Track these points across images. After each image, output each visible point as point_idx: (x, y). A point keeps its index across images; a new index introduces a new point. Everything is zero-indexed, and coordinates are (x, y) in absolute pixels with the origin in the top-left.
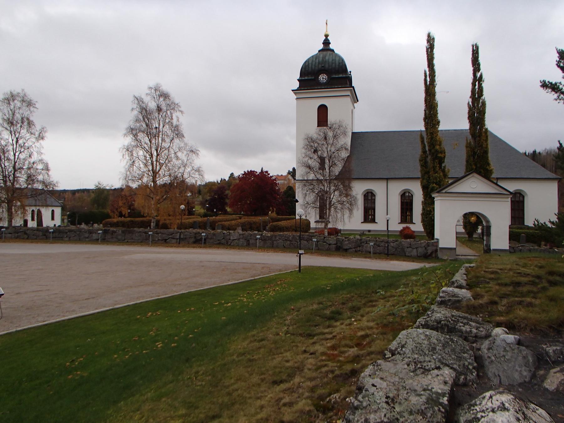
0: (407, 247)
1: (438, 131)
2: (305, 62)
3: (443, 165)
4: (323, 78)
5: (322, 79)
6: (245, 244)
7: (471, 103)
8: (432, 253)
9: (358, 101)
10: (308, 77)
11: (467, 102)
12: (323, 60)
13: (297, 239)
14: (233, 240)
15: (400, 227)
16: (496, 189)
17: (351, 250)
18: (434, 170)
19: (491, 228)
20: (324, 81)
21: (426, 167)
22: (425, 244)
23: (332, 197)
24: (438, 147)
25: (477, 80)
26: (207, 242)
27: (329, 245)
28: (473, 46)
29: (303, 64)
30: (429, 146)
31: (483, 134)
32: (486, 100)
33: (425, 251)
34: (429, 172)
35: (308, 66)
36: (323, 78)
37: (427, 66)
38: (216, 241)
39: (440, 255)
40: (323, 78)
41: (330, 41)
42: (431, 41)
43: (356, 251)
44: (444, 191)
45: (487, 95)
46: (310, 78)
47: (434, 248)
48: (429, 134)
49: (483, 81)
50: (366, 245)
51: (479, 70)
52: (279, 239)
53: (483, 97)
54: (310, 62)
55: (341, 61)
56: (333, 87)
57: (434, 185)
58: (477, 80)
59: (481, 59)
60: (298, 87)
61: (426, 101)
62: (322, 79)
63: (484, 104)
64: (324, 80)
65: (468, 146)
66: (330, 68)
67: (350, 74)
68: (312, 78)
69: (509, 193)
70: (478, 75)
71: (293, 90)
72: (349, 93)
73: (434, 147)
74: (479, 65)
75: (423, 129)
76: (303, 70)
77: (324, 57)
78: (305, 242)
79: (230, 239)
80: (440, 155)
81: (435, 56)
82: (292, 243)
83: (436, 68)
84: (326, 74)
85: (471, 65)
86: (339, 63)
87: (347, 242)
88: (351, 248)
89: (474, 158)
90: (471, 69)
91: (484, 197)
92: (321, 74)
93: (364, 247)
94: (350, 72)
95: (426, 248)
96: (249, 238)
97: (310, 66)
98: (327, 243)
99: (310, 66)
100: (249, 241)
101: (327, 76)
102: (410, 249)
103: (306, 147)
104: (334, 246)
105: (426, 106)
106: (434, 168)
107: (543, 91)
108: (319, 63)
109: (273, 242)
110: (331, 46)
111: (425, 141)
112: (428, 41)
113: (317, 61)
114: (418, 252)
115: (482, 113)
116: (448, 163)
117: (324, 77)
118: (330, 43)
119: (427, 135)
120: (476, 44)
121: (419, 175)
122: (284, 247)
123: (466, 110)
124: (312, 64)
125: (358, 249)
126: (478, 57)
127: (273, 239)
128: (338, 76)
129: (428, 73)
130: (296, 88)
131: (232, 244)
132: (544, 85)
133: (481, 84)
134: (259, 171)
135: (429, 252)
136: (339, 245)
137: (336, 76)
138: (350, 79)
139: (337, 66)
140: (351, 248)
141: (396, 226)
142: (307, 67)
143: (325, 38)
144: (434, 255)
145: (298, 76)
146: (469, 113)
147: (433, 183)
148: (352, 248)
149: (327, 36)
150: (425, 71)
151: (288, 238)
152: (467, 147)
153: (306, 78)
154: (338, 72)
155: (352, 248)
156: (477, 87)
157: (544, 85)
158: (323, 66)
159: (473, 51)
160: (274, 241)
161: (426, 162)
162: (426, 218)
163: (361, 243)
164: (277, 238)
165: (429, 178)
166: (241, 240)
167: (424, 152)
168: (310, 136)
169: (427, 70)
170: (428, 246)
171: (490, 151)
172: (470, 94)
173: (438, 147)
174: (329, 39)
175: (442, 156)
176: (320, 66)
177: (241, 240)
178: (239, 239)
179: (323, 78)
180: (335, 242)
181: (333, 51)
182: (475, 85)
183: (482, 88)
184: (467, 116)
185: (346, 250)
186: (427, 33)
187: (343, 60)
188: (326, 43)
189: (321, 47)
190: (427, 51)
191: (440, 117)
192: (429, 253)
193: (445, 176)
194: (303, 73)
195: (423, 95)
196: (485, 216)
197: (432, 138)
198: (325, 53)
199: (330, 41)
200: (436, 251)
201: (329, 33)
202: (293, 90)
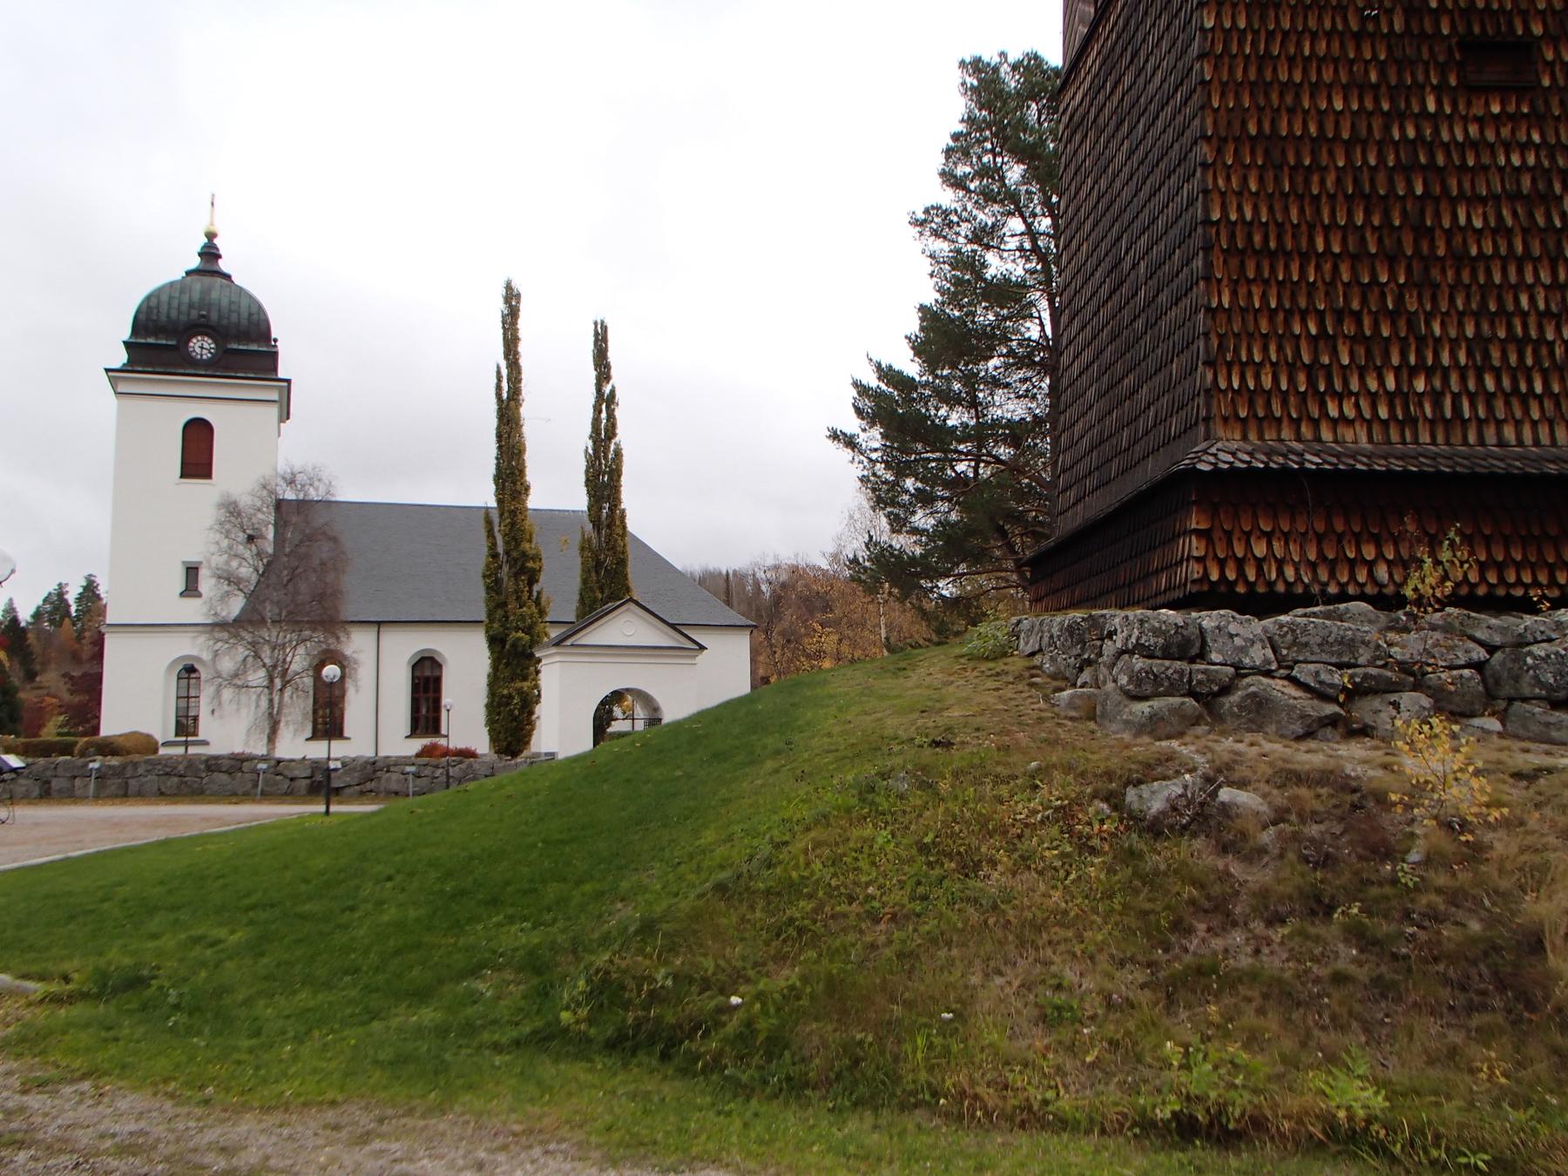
1: (527, 510)
2: (148, 298)
3: (536, 588)
4: (202, 348)
5: (198, 350)
6: (36, 792)
7: (591, 451)
9: (288, 381)
12: (202, 299)
15: (417, 745)
16: (669, 636)
17: (347, 791)
18: (518, 598)
20: (206, 355)
21: (498, 593)
23: (288, 659)
24: (526, 546)
25: (605, 401)
28: (596, 324)
29: (143, 302)
30: (506, 543)
31: (618, 523)
32: (623, 445)
34: (505, 604)
35: (158, 308)
40: (202, 348)
41: (221, 252)
42: (512, 299)
43: (362, 793)
44: (568, 642)
45: (625, 436)
46: (164, 342)
48: (506, 514)
51: (608, 378)
52: (148, 771)
53: (616, 440)
54: (165, 298)
55: (254, 310)
57: (520, 634)
58: (605, 401)
59: (612, 356)
60: (125, 361)
61: (499, 436)
62: (198, 350)
63: (618, 454)
64: (205, 351)
65: (585, 546)
66: (225, 322)
67: (275, 346)
71: (107, 370)
72: (274, 396)
73: (518, 544)
74: (608, 366)
75: (492, 502)
77: (206, 292)
78: (224, 777)
80: (530, 564)
81: (521, 334)
83: (523, 362)
85: (592, 366)
86: (250, 315)
88: (349, 786)
89: (597, 573)
90: (592, 374)
91: (606, 655)
92: (195, 335)
93: (383, 781)
94: (275, 340)
96: (49, 773)
97: (164, 309)
98: (285, 777)
99: (164, 309)
100: (48, 782)
103: (216, 527)
105: (500, 448)
106: (518, 593)
107: (832, 446)
109: (127, 783)
110: (224, 265)
111: (496, 529)
113: (186, 299)
115: (616, 473)
116: (544, 584)
117: (206, 346)
118: (219, 256)
119: (501, 515)
120: (602, 322)
121: (483, 616)
123: (582, 464)
124: (169, 304)
125: (369, 786)
126: (606, 350)
127: (129, 772)
128: (245, 348)
129: (504, 372)
130: (118, 365)
132: (835, 436)
134: (81, 590)
136: (319, 777)
137: (241, 347)
138: (272, 357)
140: (349, 786)
141: (400, 744)
142: (155, 311)
145: (126, 333)
146: (587, 472)
147: (517, 629)
149: (211, 236)
150: (498, 367)
152: (582, 549)
153: (151, 340)
156: (604, 415)
157: (835, 436)
158: (203, 316)
159: (596, 334)
160: (132, 777)
161: (498, 581)
162: (499, 714)
163: (375, 771)
165: (507, 617)
167: (495, 556)
168: (233, 499)
169: (503, 364)
171: (630, 557)
172: (588, 429)
173: (526, 546)
175: (536, 566)
176: (194, 314)
179: (201, 347)
180: (308, 773)
181: (228, 277)
182: (600, 412)
183: (614, 418)
184: (583, 478)
187: (260, 308)
188: (210, 253)
189: (195, 262)
190: (504, 323)
191: (531, 476)
193: (542, 613)
194: (139, 326)
195: (493, 422)
197: (513, 524)
198: (207, 280)
199: (221, 252)
201: (217, 228)
202: (107, 370)
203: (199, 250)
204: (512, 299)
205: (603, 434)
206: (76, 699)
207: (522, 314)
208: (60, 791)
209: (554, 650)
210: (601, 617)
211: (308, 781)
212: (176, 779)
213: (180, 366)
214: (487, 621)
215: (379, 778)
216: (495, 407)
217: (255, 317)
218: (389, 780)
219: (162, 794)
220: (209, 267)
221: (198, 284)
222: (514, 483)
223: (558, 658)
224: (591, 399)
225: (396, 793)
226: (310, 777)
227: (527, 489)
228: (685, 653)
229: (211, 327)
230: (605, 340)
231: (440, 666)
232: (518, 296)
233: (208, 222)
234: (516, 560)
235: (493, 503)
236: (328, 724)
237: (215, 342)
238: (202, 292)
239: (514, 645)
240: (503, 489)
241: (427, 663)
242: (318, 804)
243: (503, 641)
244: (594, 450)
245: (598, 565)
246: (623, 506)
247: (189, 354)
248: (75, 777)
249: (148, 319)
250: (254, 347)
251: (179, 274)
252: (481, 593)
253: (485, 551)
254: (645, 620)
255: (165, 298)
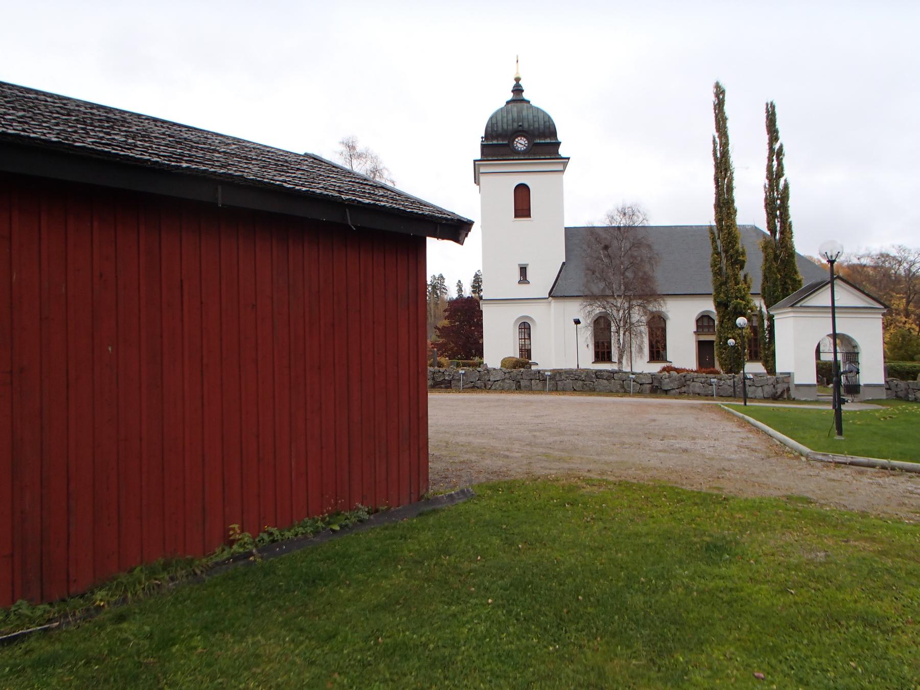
0: (750, 386)
2: (491, 118)
7: (767, 186)
8: (783, 393)
9: (568, 158)
10: (497, 141)
11: (764, 184)
12: (518, 116)
13: (592, 377)
14: (495, 381)
16: (863, 300)
17: (674, 391)
19: (860, 355)
21: (720, 275)
22: (773, 380)
26: (452, 386)
27: (641, 384)
28: (767, 105)
31: (788, 231)
33: (774, 391)
35: (497, 123)
36: (521, 143)
37: (715, 130)
38: (467, 384)
39: (793, 394)
42: (720, 93)
43: (680, 393)
44: (798, 305)
45: (790, 174)
46: (501, 142)
47: (785, 386)
49: (784, 155)
50: (693, 383)
51: (777, 139)
52: (567, 377)
54: (499, 118)
55: (546, 119)
56: (538, 157)
59: (779, 125)
66: (532, 128)
68: (504, 142)
69: (883, 307)
70: (777, 146)
71: (475, 161)
72: (560, 168)
74: (776, 131)
76: (490, 129)
77: (520, 112)
78: (605, 382)
79: (489, 380)
80: (741, 258)
82: (586, 384)
83: (730, 133)
84: (525, 137)
85: (766, 132)
87: (668, 380)
88: (673, 389)
91: (852, 313)
92: (517, 137)
93: (690, 387)
95: (774, 386)
96: (519, 377)
98: (638, 383)
99: (500, 124)
100: (519, 382)
101: (527, 140)
102: (754, 388)
104: (649, 386)
108: (513, 121)
112: (717, 95)
113: (510, 117)
114: (765, 393)
117: (523, 143)
118: (523, 91)
120: (772, 103)
121: (711, 290)
122: (575, 390)
125: (684, 389)
127: (558, 378)
128: (544, 141)
131: (493, 387)
133: (782, 159)
135: (779, 391)
136: (656, 384)
137: (541, 141)
139: (542, 127)
140: (673, 389)
143: (515, 83)
144: (785, 396)
147: (737, 298)
148: (674, 389)
149: (518, 80)
151: (580, 376)
153: (495, 142)
154: (543, 135)
155: (674, 389)
156: (775, 163)
158: (520, 126)
159: (768, 111)
163: (686, 381)
164: (563, 377)
166: (507, 381)
169: (716, 135)
170: (777, 382)
174: (522, 85)
176: (515, 125)
177: (507, 381)
178: (503, 380)
179: (521, 143)
180: (650, 381)
181: (529, 102)
185: (666, 392)
186: (713, 84)
188: (518, 90)
189: (510, 96)
192: (779, 393)
196: (848, 336)
198: (519, 105)
200: (788, 389)
201: (521, 76)
203: (512, 89)
204: (720, 93)
205: (774, 175)
206: (441, 341)
207: (726, 103)
208: (525, 387)
209: (790, 309)
210: (820, 288)
211: (650, 386)
212: (581, 382)
213: (511, 155)
214: (714, 293)
215: (689, 385)
216: (713, 163)
217: (548, 123)
218: (694, 386)
219: (575, 390)
220: (518, 98)
221: (515, 108)
222: (729, 209)
223: (792, 315)
224: (766, 153)
225: (699, 394)
226: (652, 383)
227: (736, 211)
228: (873, 311)
229: (523, 131)
230: (774, 114)
231: (665, 321)
232: (723, 92)
233: (515, 73)
234: (732, 256)
235: (714, 223)
236: (657, 352)
237: (527, 140)
238: (518, 112)
239: (735, 308)
240: (721, 212)
241: (706, 320)
242: (741, 402)
243: (726, 306)
244: (770, 185)
245: (776, 257)
246: (790, 220)
247: (514, 148)
248: (531, 380)
249: (493, 130)
250: (548, 141)
251: (503, 104)
252: (710, 276)
253: (711, 251)
254: (846, 289)
255: (499, 118)
